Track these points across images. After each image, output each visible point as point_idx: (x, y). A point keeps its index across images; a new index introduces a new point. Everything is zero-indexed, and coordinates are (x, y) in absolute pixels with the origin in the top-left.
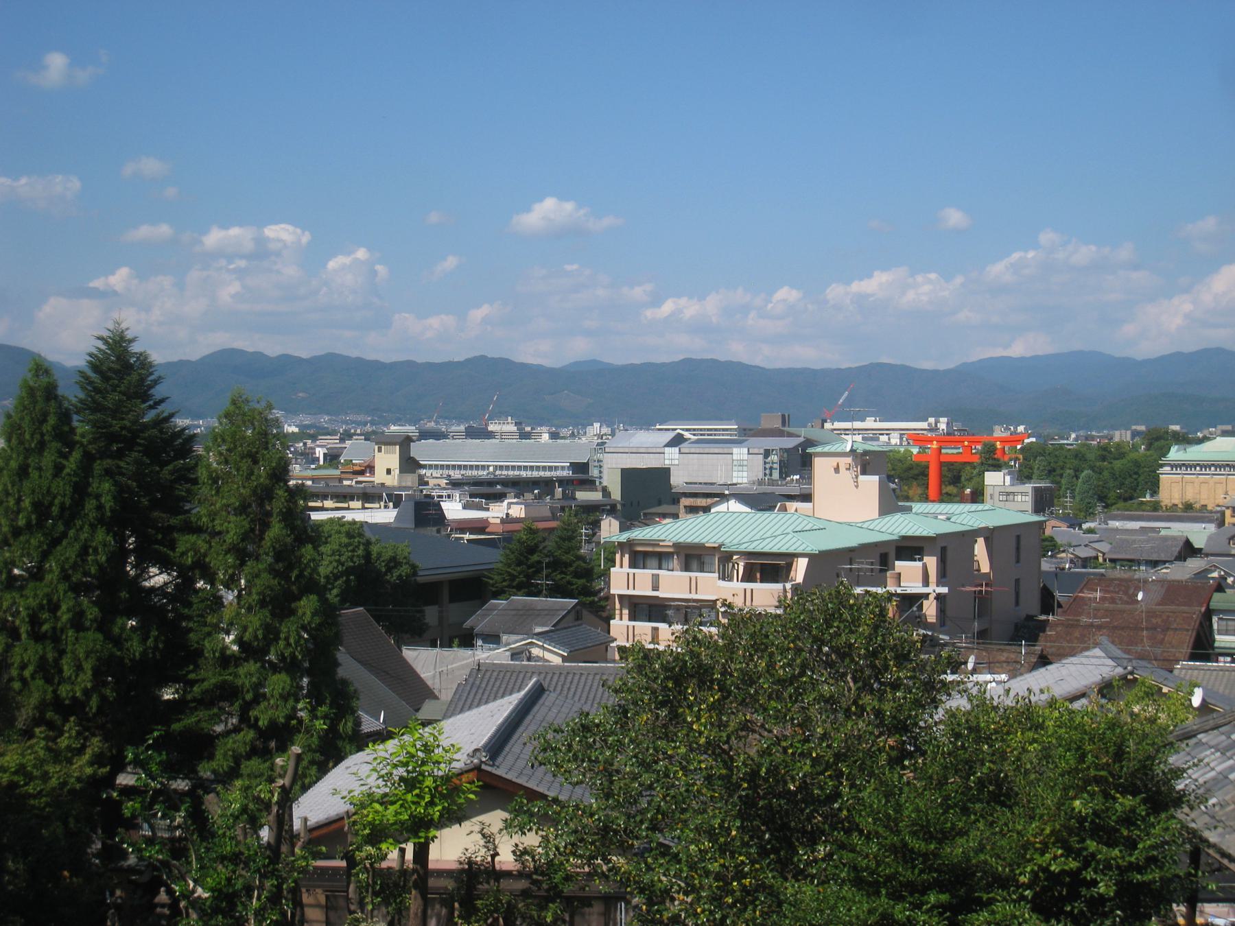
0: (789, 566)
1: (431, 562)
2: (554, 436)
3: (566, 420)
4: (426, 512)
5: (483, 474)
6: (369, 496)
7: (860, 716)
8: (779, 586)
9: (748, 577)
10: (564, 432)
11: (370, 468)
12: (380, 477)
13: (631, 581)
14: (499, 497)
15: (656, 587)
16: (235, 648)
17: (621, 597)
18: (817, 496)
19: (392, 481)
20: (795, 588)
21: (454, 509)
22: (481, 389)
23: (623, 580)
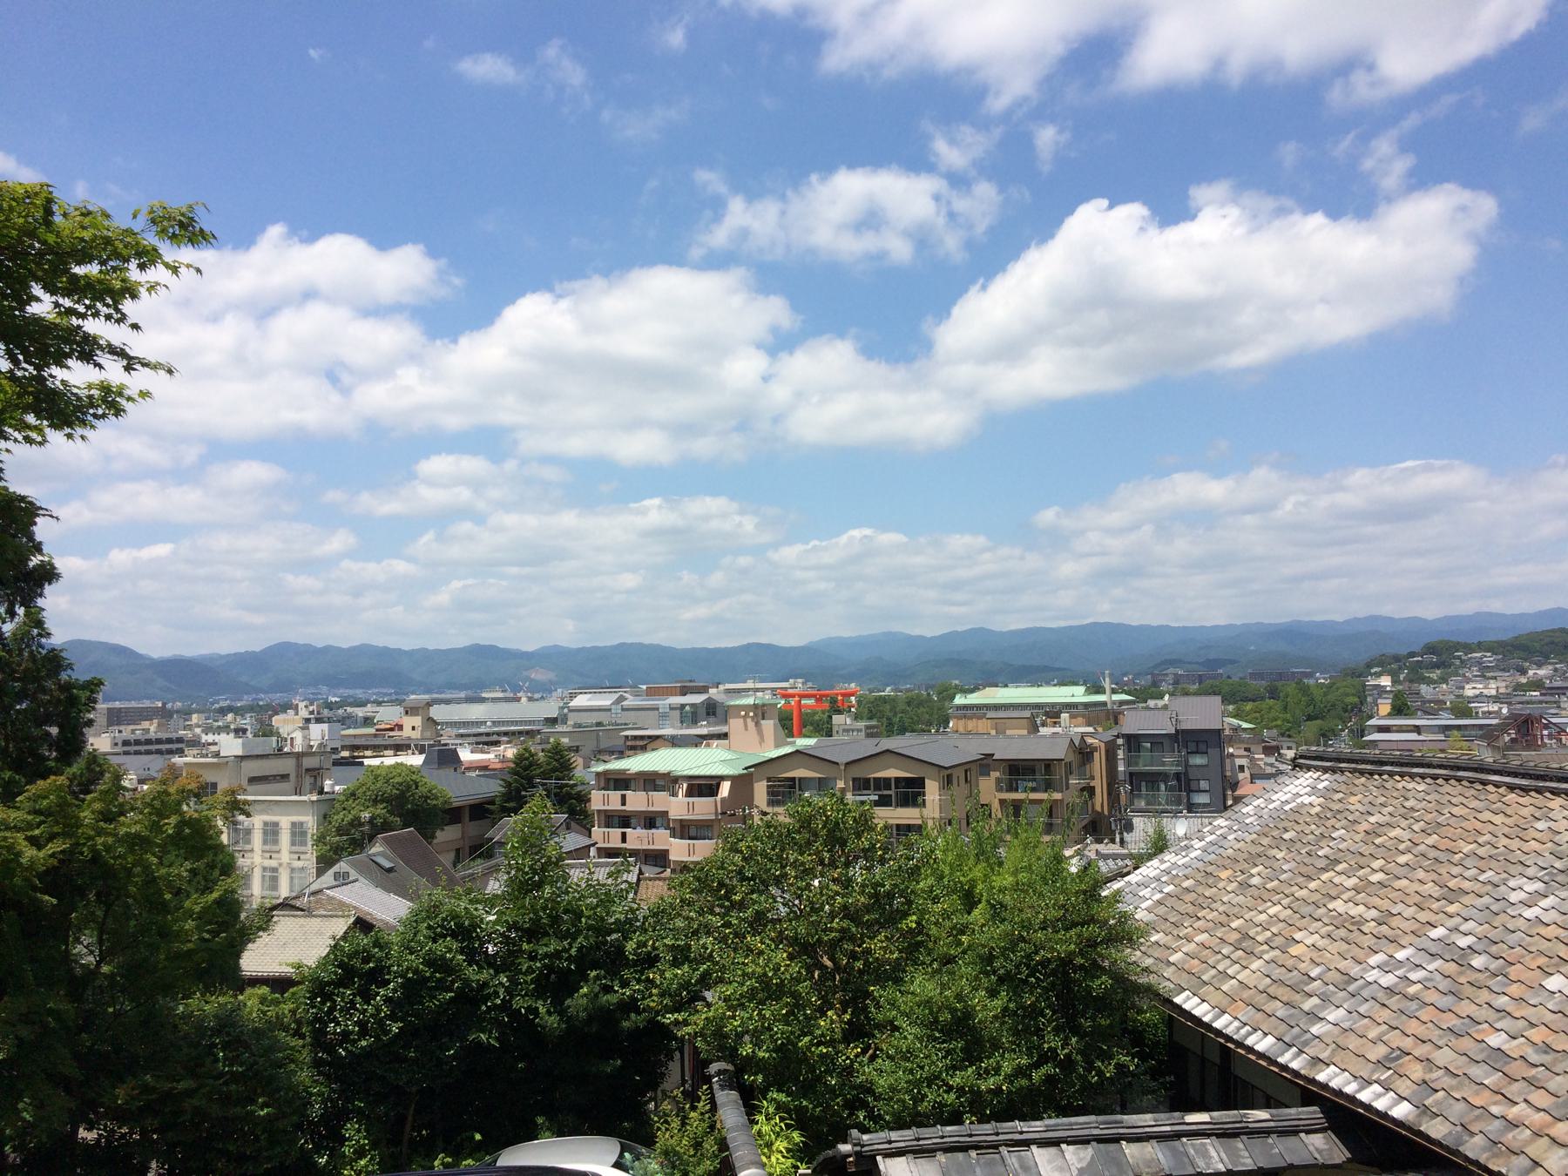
0: (718, 785)
1: (454, 789)
2: (530, 699)
3: (541, 691)
4: (447, 758)
5: (482, 730)
6: (399, 748)
7: (954, 927)
8: (711, 799)
9: (689, 794)
10: (537, 696)
11: (400, 727)
12: (407, 732)
13: (606, 800)
14: (497, 743)
15: (624, 804)
16: (540, 1120)
17: (599, 811)
18: (731, 736)
19: (416, 735)
20: (723, 800)
21: (466, 755)
22: (484, 669)
23: (601, 800)
